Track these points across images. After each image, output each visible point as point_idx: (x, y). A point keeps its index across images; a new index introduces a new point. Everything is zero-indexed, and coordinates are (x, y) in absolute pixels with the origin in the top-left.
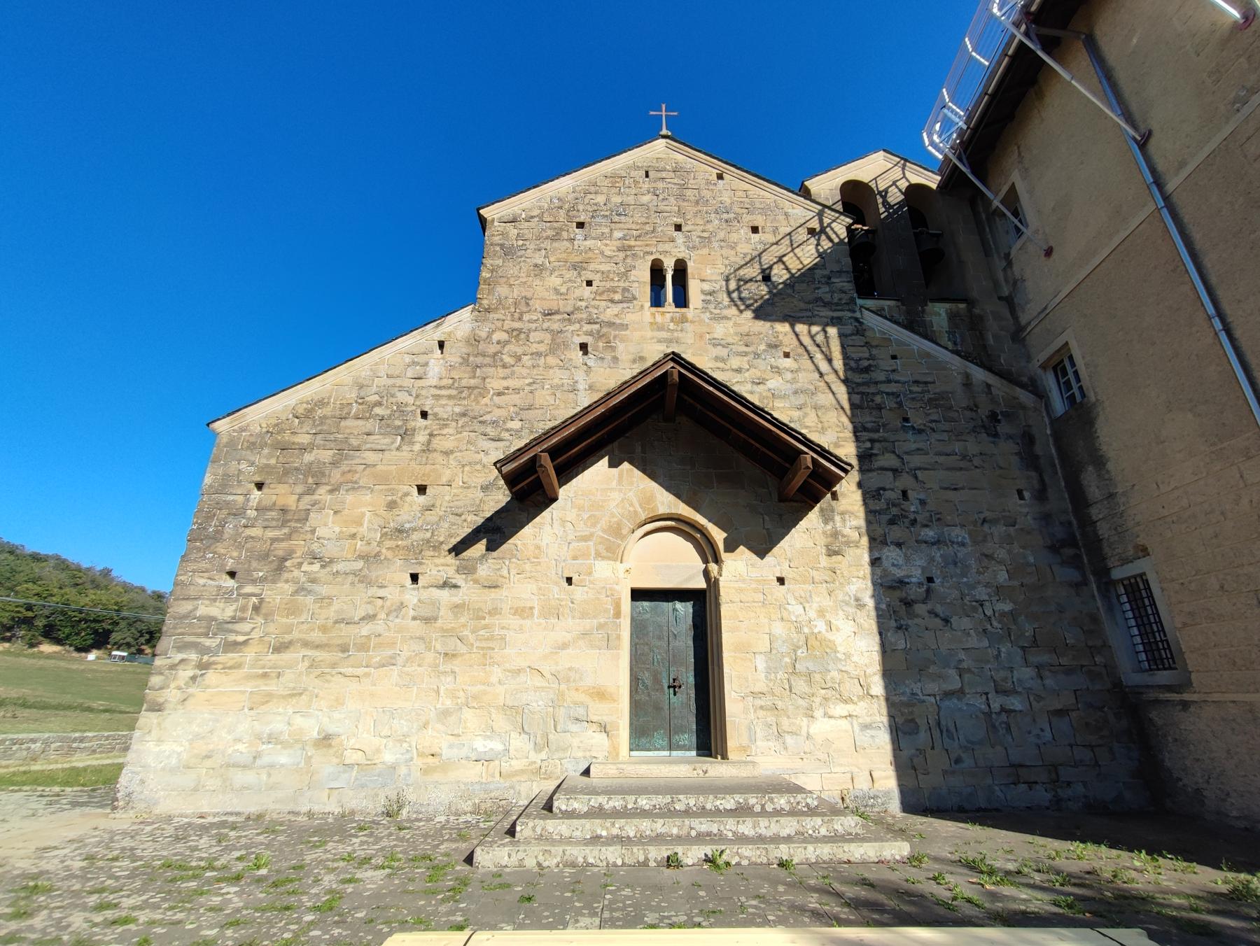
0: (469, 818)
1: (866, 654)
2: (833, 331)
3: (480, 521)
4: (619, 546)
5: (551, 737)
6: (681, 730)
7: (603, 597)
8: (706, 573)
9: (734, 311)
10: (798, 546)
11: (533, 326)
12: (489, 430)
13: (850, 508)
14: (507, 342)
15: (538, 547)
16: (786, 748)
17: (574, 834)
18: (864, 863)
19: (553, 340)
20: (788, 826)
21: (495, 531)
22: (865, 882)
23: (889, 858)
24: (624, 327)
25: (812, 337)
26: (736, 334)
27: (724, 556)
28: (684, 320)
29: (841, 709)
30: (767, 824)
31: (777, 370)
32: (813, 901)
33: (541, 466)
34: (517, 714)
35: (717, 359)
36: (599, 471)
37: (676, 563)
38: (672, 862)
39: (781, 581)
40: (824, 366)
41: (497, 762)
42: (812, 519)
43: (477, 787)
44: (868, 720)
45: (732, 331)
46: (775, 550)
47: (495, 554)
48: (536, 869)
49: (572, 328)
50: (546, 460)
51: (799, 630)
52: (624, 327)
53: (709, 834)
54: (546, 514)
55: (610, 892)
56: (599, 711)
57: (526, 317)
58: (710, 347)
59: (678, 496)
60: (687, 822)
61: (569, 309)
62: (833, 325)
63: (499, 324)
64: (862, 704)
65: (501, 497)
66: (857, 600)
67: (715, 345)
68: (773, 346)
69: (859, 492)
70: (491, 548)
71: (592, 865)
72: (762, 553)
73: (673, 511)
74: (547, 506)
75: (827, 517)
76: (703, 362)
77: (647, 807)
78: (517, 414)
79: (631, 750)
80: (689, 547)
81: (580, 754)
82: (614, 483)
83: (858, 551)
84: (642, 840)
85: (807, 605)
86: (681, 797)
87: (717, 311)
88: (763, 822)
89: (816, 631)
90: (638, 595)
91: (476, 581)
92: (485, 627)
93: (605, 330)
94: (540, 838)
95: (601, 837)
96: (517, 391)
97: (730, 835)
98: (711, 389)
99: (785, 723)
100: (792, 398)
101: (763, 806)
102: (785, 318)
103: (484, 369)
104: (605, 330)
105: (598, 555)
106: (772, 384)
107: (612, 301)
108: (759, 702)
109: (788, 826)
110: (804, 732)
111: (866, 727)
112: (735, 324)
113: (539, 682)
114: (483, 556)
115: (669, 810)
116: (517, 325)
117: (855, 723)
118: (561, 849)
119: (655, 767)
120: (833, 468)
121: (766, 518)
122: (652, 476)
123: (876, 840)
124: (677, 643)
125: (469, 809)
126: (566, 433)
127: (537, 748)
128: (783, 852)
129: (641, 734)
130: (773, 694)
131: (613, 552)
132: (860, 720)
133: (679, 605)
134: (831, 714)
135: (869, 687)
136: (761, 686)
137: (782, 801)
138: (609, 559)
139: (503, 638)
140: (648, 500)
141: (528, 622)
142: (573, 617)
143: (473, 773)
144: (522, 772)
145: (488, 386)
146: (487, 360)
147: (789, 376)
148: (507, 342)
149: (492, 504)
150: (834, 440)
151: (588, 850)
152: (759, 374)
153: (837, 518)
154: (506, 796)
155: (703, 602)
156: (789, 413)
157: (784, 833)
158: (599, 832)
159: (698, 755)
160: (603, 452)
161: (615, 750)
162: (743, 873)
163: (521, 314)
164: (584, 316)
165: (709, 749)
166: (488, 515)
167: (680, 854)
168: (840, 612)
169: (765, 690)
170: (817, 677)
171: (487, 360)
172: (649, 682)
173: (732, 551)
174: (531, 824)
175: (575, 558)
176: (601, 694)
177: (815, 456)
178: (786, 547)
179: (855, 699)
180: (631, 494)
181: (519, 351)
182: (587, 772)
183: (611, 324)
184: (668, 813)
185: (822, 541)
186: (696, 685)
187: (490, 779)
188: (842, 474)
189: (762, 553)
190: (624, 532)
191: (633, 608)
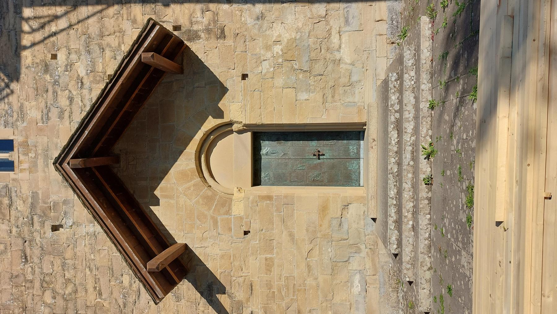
0: (401, 295)
1: (297, 16)
2: (27, 12)
3: (203, 301)
4: (221, 197)
5: (351, 242)
6: (347, 151)
7: (258, 209)
8: (240, 132)
9: (12, 99)
10: (218, 61)
11: (37, 270)
12: (131, 299)
13: (187, 17)
14: (54, 291)
15: (222, 257)
16: (360, 81)
17: (411, 242)
18: (433, 50)
19: (50, 254)
20: (409, 98)
21: (210, 288)
22: (444, 56)
23: (430, 32)
24: (35, 195)
25: (33, 31)
26: (36, 100)
27: (226, 120)
28: (25, 144)
29: (335, 39)
30: (407, 113)
31: (69, 66)
32: (453, 99)
33: (157, 268)
34: (335, 267)
35: (61, 116)
36: (162, 213)
37: (233, 152)
38: (429, 182)
39: (244, 77)
40: (62, 23)
41: (367, 278)
42: (196, 47)
43: (382, 290)
44: (342, 19)
45: (34, 103)
46: (221, 79)
47: (228, 288)
48: (432, 271)
49: (38, 239)
50: (153, 264)
51: (280, 65)
52: (35, 195)
53: (412, 153)
54: (197, 252)
55: (447, 232)
56: (334, 210)
57: (29, 277)
58: (50, 123)
59: (181, 152)
60: (405, 167)
61: (20, 241)
62: (21, 12)
63: (37, 299)
64: (331, 23)
65: (185, 287)
66: (258, 19)
67: (48, 118)
68: (47, 69)
69: (172, 6)
70: (223, 291)
71: (430, 234)
72: (224, 90)
73: (193, 156)
74: (191, 251)
75: (195, 36)
76: (64, 130)
77: (395, 191)
78: (117, 279)
79: (359, 185)
80: (221, 144)
81: (362, 222)
82: (172, 201)
83: (221, 14)
84: (415, 198)
85: (262, 58)
86: (389, 168)
87: (15, 115)
88: (406, 115)
89: (281, 53)
90: (256, 181)
91: (248, 300)
92: (279, 291)
93: (39, 211)
94: (413, 265)
95: (413, 225)
96: (97, 280)
97: (413, 138)
98: (86, 132)
99: (343, 80)
100: (94, 55)
101: (396, 112)
102: (17, 56)
103: (79, 307)
104: (39, 211)
105: (228, 212)
106: (82, 72)
107: (10, 206)
108: (330, 99)
109: (409, 98)
110: (350, 67)
111: (347, 21)
112: (27, 99)
113: (316, 252)
114: (230, 296)
115: (397, 176)
116: (37, 284)
117: (343, 29)
118: (420, 255)
119: (370, 175)
120: (152, 35)
121: (197, 85)
122: (165, 172)
123: (419, 39)
124: (290, 153)
125: (395, 294)
126: (130, 250)
127: (359, 251)
128: (424, 106)
129: (349, 179)
130: (324, 88)
131: (226, 202)
132: (342, 25)
133: (264, 151)
134: (337, 47)
135: (320, 16)
136: (318, 96)
137: (393, 98)
138: (230, 205)
139: (287, 278)
140: (184, 175)
141: (276, 261)
142: (272, 229)
143: (374, 293)
144: (373, 260)
145: (93, 303)
146: (71, 305)
147: (74, 57)
148: (54, 291)
149: (190, 293)
150: (129, 23)
151: (421, 238)
152: (73, 83)
153: (195, 27)
154: (388, 271)
155: (259, 135)
156: (107, 59)
157: (413, 101)
158: (410, 226)
159: (363, 139)
160: (147, 211)
161: (361, 200)
162: (436, 138)
163: (26, 281)
164: (26, 229)
165: (360, 132)
166: (199, 295)
167: (424, 176)
168: (268, 32)
169: (321, 94)
170: (313, 55)
171: (71, 305)
172: (316, 173)
173: (222, 112)
174: (405, 271)
175: (230, 229)
176: (324, 209)
177: (142, 49)
178: (219, 70)
179: (328, 27)
180: (180, 189)
181: (61, 280)
182: (374, 220)
183: (33, 206)
184: (399, 176)
185: (213, 42)
186: (318, 140)
187: (378, 282)
188: (157, 27)
189: (224, 90)
190: (210, 193)
191: (264, 185)
